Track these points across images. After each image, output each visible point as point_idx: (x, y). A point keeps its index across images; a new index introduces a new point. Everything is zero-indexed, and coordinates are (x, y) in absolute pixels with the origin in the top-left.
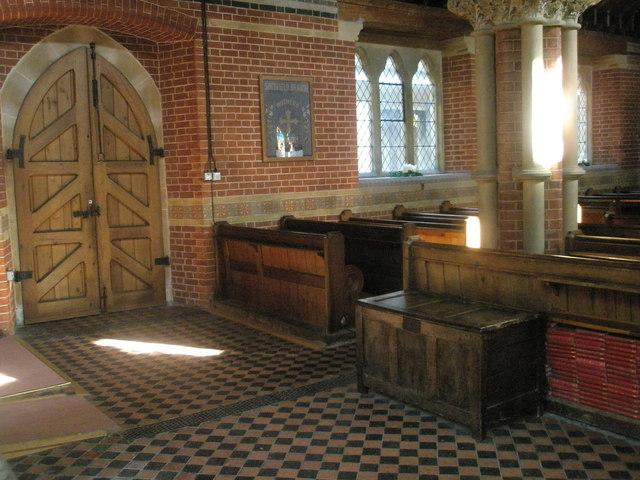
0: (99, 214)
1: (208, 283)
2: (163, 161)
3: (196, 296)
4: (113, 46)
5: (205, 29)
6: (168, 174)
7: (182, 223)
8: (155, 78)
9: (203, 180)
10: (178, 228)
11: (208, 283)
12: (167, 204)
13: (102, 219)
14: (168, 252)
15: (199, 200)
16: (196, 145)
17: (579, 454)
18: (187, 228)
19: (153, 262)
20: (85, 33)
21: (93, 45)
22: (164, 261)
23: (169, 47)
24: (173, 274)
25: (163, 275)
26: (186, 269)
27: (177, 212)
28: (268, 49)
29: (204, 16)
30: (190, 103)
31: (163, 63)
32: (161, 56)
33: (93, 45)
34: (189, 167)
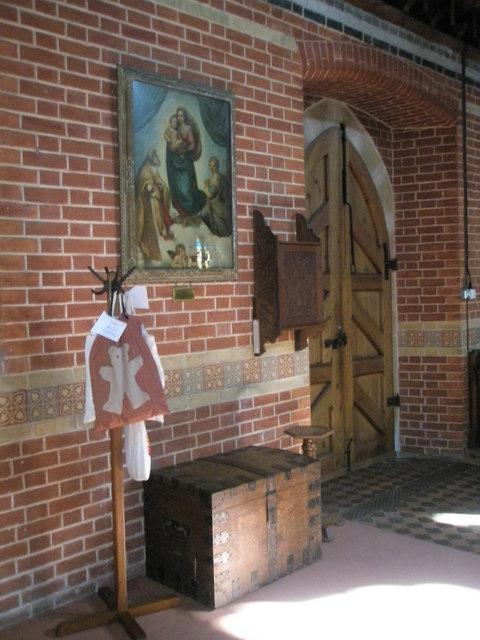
0: (346, 342)
1: (459, 428)
2: (394, 274)
3: (443, 444)
4: (358, 129)
5: (464, 114)
6: (399, 292)
7: (422, 352)
8: (390, 172)
9: (461, 298)
10: (415, 359)
11: (459, 428)
12: (398, 328)
13: (348, 350)
14: (397, 390)
15: (455, 323)
16: (453, 255)
17: (431, 535)
18: (428, 359)
19: (385, 402)
20: (337, 107)
21: (343, 127)
22: (395, 401)
23: (410, 135)
24: (402, 416)
25: (393, 415)
26: (426, 409)
27: (412, 339)
28: (281, 150)
29: (464, 99)
30: (446, 203)
31: (397, 154)
32: (396, 145)
33: (343, 127)
34: (440, 283)
